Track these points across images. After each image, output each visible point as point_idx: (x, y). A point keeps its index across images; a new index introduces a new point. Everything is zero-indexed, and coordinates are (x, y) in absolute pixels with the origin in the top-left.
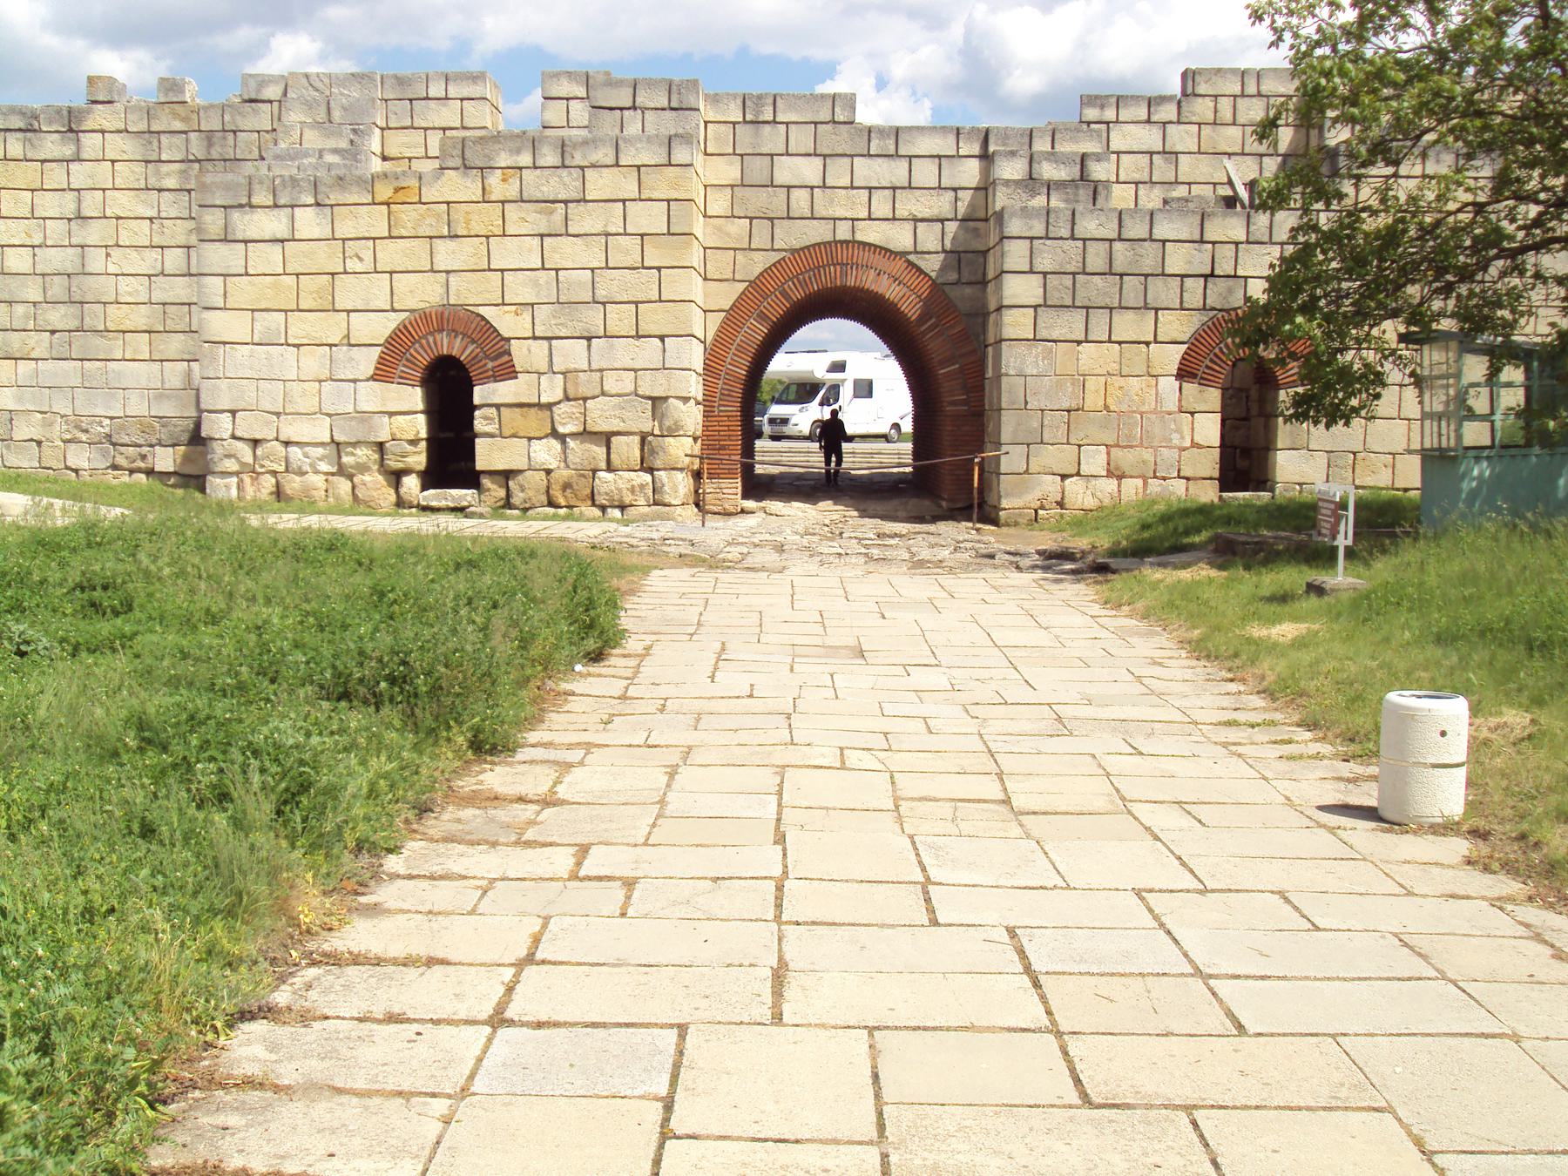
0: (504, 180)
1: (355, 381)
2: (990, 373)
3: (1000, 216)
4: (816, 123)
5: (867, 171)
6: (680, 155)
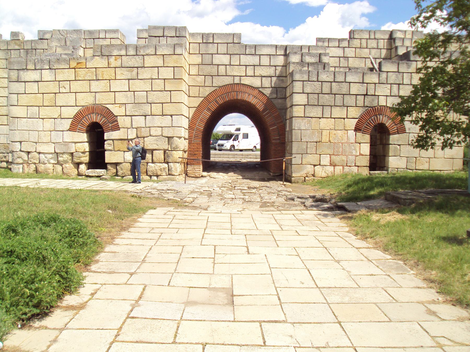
0: (115, 60)
1: (63, 131)
2: (288, 129)
3: (292, 74)
4: (227, 43)
5: (246, 60)
6: (178, 51)
